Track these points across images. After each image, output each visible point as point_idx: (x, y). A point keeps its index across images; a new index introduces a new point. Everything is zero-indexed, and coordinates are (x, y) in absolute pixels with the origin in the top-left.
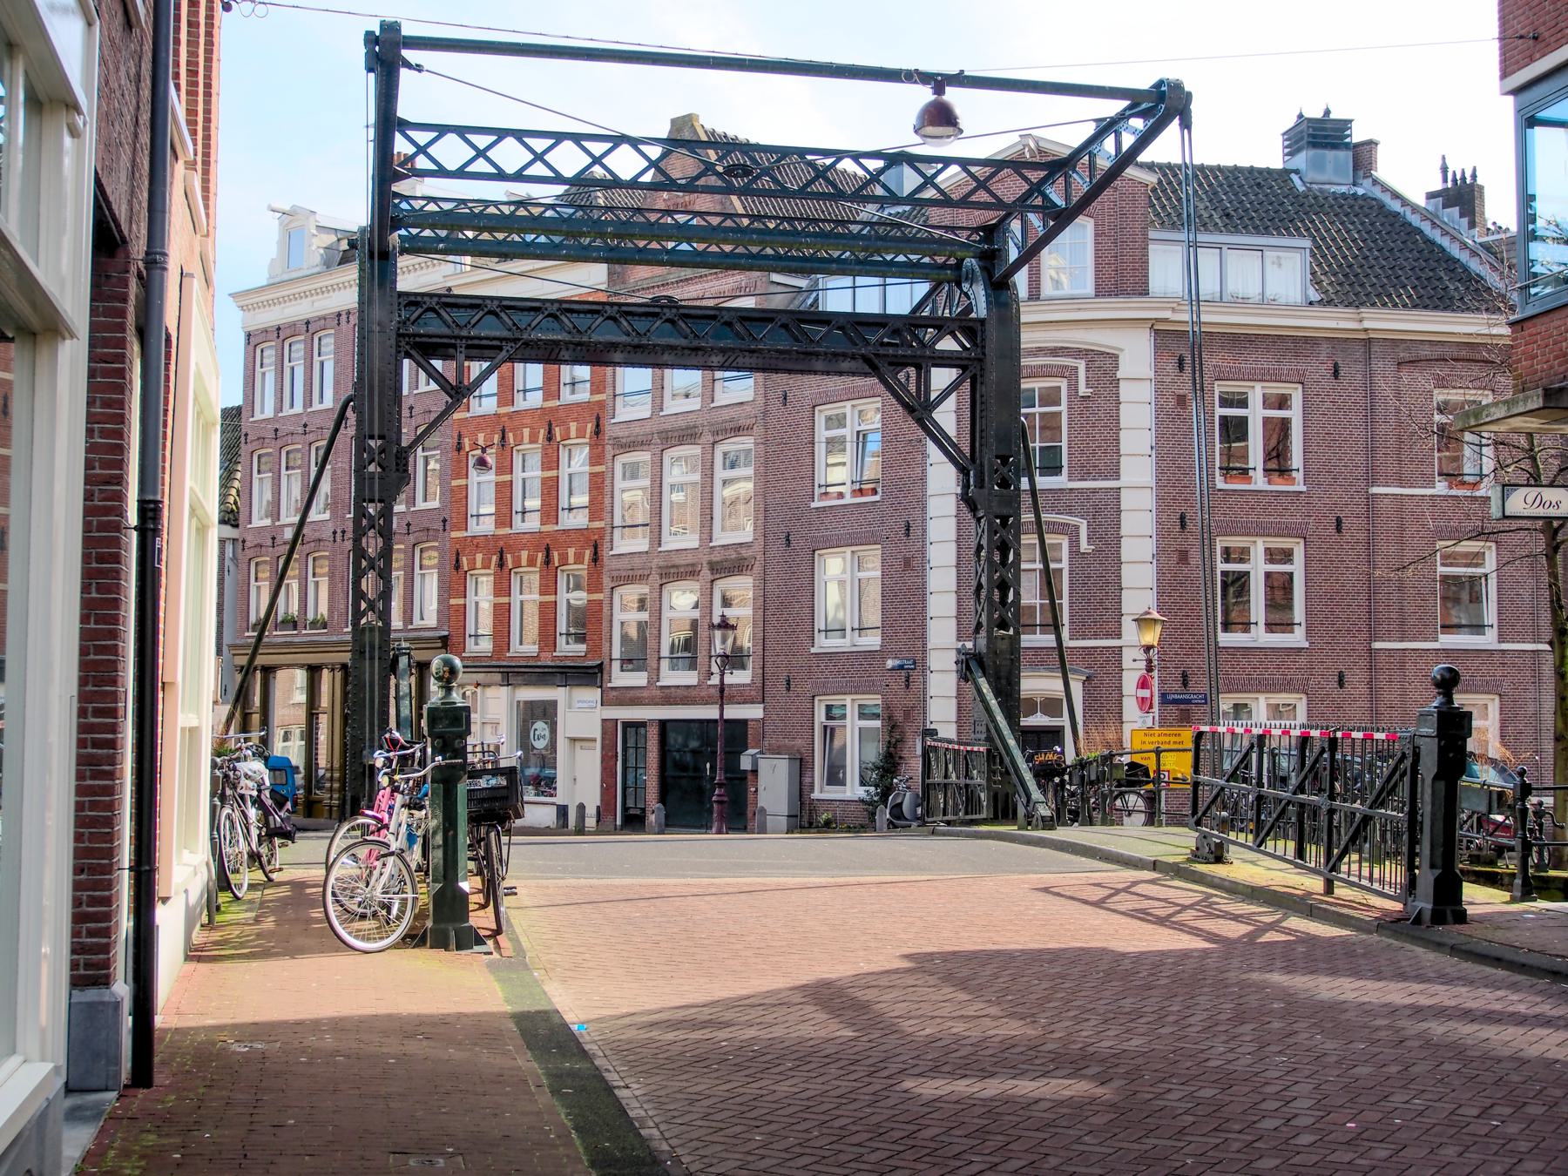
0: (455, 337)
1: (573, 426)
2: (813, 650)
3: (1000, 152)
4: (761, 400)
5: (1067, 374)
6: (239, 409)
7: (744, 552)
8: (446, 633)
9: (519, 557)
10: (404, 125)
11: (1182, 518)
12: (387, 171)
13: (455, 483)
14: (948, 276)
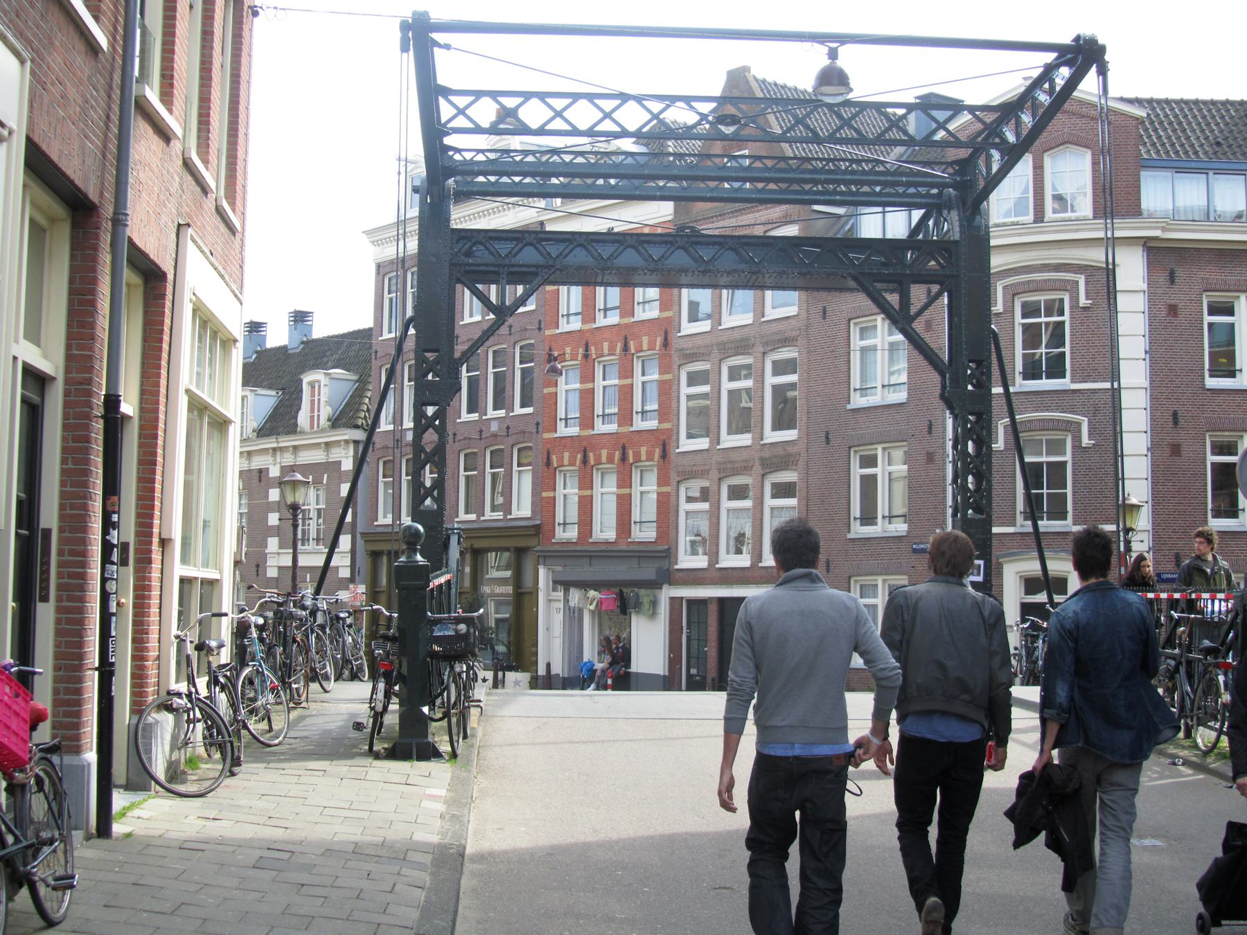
0: (499, 266)
1: (645, 340)
2: (849, 536)
3: (994, 100)
4: (804, 315)
5: (1068, 288)
6: (370, 329)
7: (790, 449)
8: (538, 522)
9: (600, 456)
10: (446, 92)
11: (1175, 415)
12: (434, 132)
13: (546, 391)
14: (934, 208)
